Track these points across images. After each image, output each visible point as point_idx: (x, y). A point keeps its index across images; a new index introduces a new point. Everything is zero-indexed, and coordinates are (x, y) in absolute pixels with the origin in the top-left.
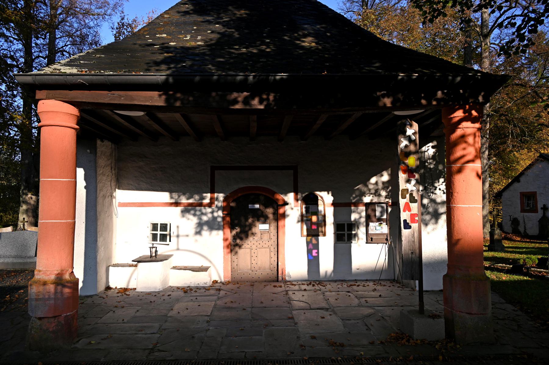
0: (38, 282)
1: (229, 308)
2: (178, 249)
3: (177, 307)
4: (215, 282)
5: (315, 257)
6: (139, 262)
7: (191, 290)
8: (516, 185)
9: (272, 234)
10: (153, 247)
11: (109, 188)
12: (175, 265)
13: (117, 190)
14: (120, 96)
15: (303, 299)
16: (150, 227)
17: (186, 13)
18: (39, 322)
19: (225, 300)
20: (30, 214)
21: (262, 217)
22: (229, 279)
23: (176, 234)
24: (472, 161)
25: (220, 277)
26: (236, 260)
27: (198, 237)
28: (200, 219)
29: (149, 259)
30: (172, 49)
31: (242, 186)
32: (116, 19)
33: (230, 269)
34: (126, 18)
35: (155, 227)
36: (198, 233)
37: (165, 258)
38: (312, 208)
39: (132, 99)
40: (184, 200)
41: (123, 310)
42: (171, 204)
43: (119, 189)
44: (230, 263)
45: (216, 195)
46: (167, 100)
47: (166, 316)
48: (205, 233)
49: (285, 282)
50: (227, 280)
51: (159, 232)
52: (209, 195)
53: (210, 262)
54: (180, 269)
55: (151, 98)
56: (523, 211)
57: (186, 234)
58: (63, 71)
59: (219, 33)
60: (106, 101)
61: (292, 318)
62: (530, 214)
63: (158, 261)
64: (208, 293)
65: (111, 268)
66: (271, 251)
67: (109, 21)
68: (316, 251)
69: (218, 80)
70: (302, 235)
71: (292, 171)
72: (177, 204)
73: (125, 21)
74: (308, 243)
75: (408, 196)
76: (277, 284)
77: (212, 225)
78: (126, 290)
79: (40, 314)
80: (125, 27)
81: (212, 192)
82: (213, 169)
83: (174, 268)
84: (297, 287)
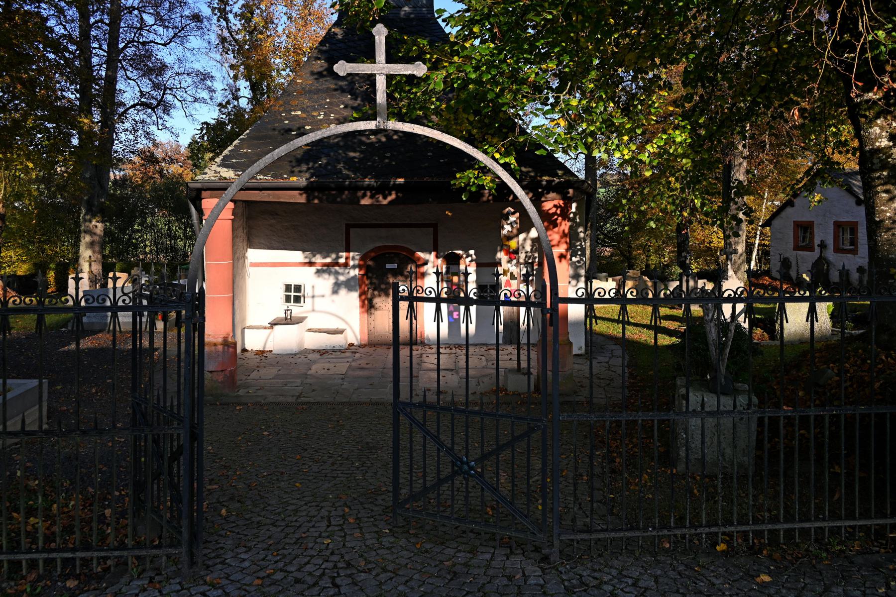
0: (209, 343)
1: (363, 369)
2: (313, 310)
3: (314, 367)
4: (351, 345)
5: (455, 319)
7: (327, 352)
8: (789, 210)
10: (288, 310)
11: (242, 249)
12: (309, 328)
13: (249, 250)
14: (269, 195)
16: (284, 288)
18: (210, 375)
20: (97, 249)
22: (365, 341)
23: (310, 294)
24: (558, 245)
25: (357, 339)
26: (373, 323)
27: (335, 297)
28: (337, 279)
29: (284, 322)
31: (378, 244)
33: (366, 331)
35: (288, 288)
36: (335, 292)
37: (299, 321)
38: (453, 268)
40: (319, 259)
41: (266, 369)
42: (305, 264)
43: (250, 248)
44: (366, 325)
45: (351, 254)
46: (308, 199)
47: (306, 374)
48: (343, 292)
50: (363, 342)
51: (293, 294)
52: (344, 254)
53: (346, 323)
54: (316, 332)
55: (294, 196)
56: (797, 248)
57: (322, 293)
60: (258, 199)
62: (805, 253)
63: (293, 324)
64: (343, 355)
65: (246, 330)
68: (457, 313)
69: (349, 185)
71: (432, 229)
72: (311, 264)
75: (509, 274)
77: (349, 285)
78: (263, 352)
79: (211, 369)
81: (348, 250)
82: (348, 227)
83: (309, 330)
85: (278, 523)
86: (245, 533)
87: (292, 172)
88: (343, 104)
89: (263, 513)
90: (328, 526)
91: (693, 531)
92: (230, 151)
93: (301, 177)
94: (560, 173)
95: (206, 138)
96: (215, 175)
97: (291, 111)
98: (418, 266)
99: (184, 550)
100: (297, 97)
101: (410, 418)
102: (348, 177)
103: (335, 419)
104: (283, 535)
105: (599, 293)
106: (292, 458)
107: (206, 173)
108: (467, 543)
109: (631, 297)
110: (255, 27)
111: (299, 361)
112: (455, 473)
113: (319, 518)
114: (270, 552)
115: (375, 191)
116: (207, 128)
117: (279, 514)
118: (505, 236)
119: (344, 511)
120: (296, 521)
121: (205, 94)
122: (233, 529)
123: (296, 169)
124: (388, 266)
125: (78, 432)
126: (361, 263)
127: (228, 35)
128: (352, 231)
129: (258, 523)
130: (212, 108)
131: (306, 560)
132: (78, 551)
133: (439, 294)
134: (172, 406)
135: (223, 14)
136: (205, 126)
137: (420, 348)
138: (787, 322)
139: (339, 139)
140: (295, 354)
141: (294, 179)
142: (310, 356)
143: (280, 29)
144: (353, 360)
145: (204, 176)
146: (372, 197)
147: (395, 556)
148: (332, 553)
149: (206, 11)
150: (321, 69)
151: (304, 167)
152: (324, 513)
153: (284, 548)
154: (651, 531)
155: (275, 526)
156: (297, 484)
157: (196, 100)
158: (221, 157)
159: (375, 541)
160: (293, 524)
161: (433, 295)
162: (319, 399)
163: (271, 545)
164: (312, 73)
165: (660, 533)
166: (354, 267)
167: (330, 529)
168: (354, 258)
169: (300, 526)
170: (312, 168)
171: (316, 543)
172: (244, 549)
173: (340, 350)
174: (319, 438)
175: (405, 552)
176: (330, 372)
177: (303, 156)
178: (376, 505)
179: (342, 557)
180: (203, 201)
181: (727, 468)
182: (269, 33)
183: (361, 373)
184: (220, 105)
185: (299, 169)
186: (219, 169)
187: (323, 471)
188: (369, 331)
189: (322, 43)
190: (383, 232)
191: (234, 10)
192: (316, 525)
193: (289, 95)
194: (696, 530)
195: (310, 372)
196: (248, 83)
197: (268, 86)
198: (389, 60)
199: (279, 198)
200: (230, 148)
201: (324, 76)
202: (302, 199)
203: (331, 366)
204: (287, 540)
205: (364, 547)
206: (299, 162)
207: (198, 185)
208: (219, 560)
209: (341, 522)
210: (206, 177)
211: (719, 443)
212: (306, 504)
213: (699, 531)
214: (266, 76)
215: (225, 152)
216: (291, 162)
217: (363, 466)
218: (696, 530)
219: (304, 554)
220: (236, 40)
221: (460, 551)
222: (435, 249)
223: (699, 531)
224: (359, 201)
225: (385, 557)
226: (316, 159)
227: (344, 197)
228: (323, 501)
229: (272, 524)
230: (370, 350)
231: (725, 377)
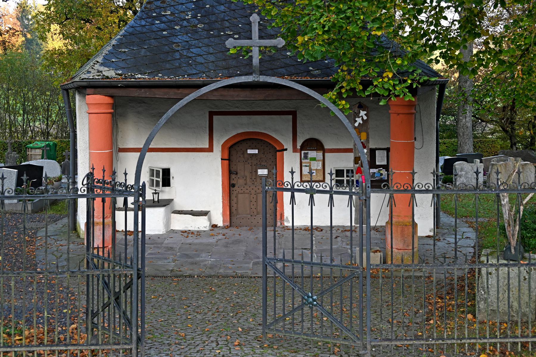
29: (152, 203)
58: (106, 74)
71: (291, 117)
82: (211, 114)
89: (170, 339)
90: (217, 345)
91: (459, 342)
95: (52, 9)
96: (98, 74)
99: (134, 346)
101: (274, 268)
103: (207, 287)
105: (397, 186)
106: (180, 311)
109: (418, 189)
112: (304, 304)
113: (210, 341)
120: (194, 343)
125: (69, 272)
128: (215, 118)
129: (168, 344)
132: (69, 346)
133: (293, 186)
138: (395, 206)
145: (88, 75)
154: (431, 341)
156: (189, 325)
161: (289, 187)
165: (437, 342)
169: (198, 345)
171: (211, 352)
174: (197, 300)
178: (249, 336)
181: (514, 316)
186: (102, 68)
187: (206, 319)
192: (209, 345)
194: (461, 341)
198: (261, 37)
209: (226, 343)
211: (509, 297)
212: (199, 335)
213: (463, 341)
217: (236, 316)
218: (461, 341)
223: (463, 341)
228: (211, 333)
231: (515, 248)
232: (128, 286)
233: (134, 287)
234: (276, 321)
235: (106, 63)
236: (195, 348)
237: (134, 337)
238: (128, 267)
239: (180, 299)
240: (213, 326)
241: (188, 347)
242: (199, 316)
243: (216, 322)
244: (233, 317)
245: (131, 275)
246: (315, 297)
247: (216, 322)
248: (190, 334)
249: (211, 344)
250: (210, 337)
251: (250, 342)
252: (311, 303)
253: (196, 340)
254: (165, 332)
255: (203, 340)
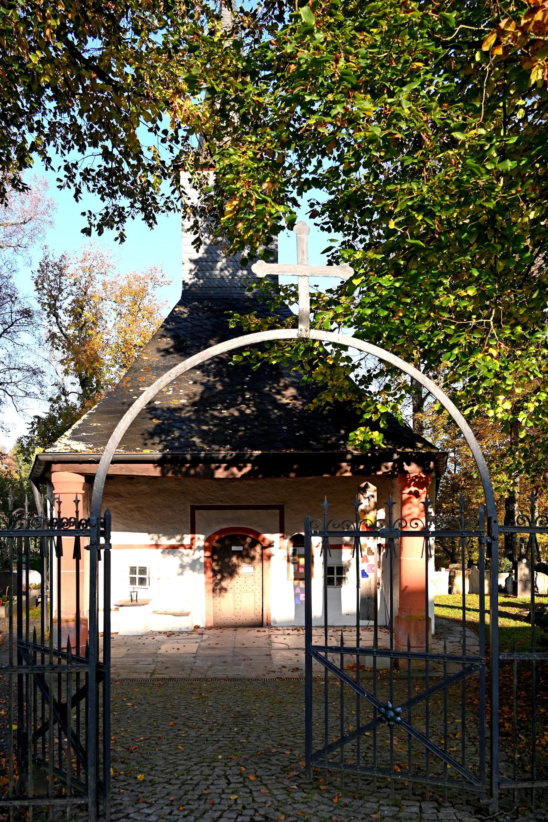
1: (213, 648)
4: (197, 627)
6: (122, 606)
7: (173, 634)
9: (257, 578)
14: (121, 468)
15: (285, 642)
16: (129, 570)
17: (167, 352)
19: (208, 642)
21: (246, 556)
22: (211, 624)
26: (218, 605)
29: (130, 603)
30: (159, 412)
31: (224, 526)
32: (37, 257)
33: (212, 613)
34: (50, 256)
35: (133, 570)
39: (131, 471)
40: (165, 541)
45: (197, 536)
46: (162, 471)
48: (188, 572)
49: (269, 625)
55: (147, 470)
58: (75, 448)
59: (202, 384)
61: (270, 655)
64: (190, 636)
66: (255, 596)
67: (25, 254)
69: (205, 457)
70: (288, 578)
71: (278, 511)
72: (157, 546)
73: (51, 258)
74: (295, 587)
76: (261, 629)
80: (51, 268)
82: (194, 509)
83: (155, 612)
84: (281, 632)
85: (173, 781)
86: (140, 790)
87: (145, 444)
88: (191, 380)
89: (153, 773)
92: (79, 425)
93: (154, 449)
94: (419, 445)
97: (139, 387)
98: (263, 548)
99: (90, 800)
100: (144, 374)
102: (203, 450)
104: (182, 792)
107: (56, 446)
108: (388, 797)
110: (85, 323)
111: (146, 641)
112: (377, 721)
114: (175, 808)
115: (231, 463)
116: (39, 422)
117: (171, 773)
118: (362, 511)
119: (240, 770)
120: (191, 779)
121: (35, 389)
122: (126, 787)
123: (149, 442)
124: (234, 548)
126: (207, 544)
127: (59, 330)
128: (197, 512)
129: (150, 781)
130: (43, 403)
131: (218, 814)
134: (69, 647)
135: (53, 310)
136: (36, 420)
137: (267, 630)
139: (191, 413)
140: (142, 636)
141: (148, 451)
142: (157, 638)
143: (110, 325)
144: (202, 641)
146: (226, 469)
147: (314, 810)
148: (244, 808)
149: (36, 306)
150: (167, 347)
151: (157, 440)
152: (218, 771)
153: (188, 804)
155: (170, 784)
157: (27, 394)
158: (70, 431)
159: (285, 797)
160: (189, 782)
162: (174, 675)
163: (172, 801)
164: (159, 350)
166: (199, 548)
167: (231, 786)
168: (200, 540)
169: (197, 784)
170: (165, 440)
171: (222, 799)
172: (145, 805)
173: (186, 632)
175: (323, 807)
176: (180, 652)
177: (155, 429)
178: (272, 765)
179: (256, 811)
180: (53, 475)
182: (98, 329)
183: (212, 652)
184: (51, 400)
185: (152, 441)
188: (215, 613)
189: (166, 321)
190: (229, 513)
191: (64, 306)
192: (215, 782)
193: (136, 371)
195: (159, 652)
196: (78, 380)
197: (98, 382)
199: (132, 471)
200: (79, 422)
201: (169, 353)
202: (153, 471)
203: (180, 646)
204: (189, 797)
205: (276, 802)
206: (152, 435)
207: (49, 458)
208: (121, 815)
209: (242, 780)
210: (57, 450)
212: (196, 764)
214: (96, 372)
215: (75, 426)
216: (143, 434)
219: (214, 808)
220: (65, 336)
221: (383, 805)
222: (282, 530)
224: (213, 474)
225: (304, 810)
226: (168, 432)
227: (198, 469)
228: (213, 762)
229: (167, 782)
230: (218, 632)
232: (82, 693)
233: (91, 695)
234: (329, 748)
235: (75, 437)
236: (193, 790)
237: (92, 784)
238: (81, 661)
239: (165, 708)
240: (214, 748)
241: (183, 787)
242: (193, 733)
243: (217, 741)
244: (238, 734)
245: (87, 674)
246: (399, 709)
247: (217, 741)
248: (182, 762)
249: (218, 782)
250: (214, 768)
251: (278, 778)
252: (392, 719)
253: (195, 773)
254: (146, 759)
255: (204, 773)
